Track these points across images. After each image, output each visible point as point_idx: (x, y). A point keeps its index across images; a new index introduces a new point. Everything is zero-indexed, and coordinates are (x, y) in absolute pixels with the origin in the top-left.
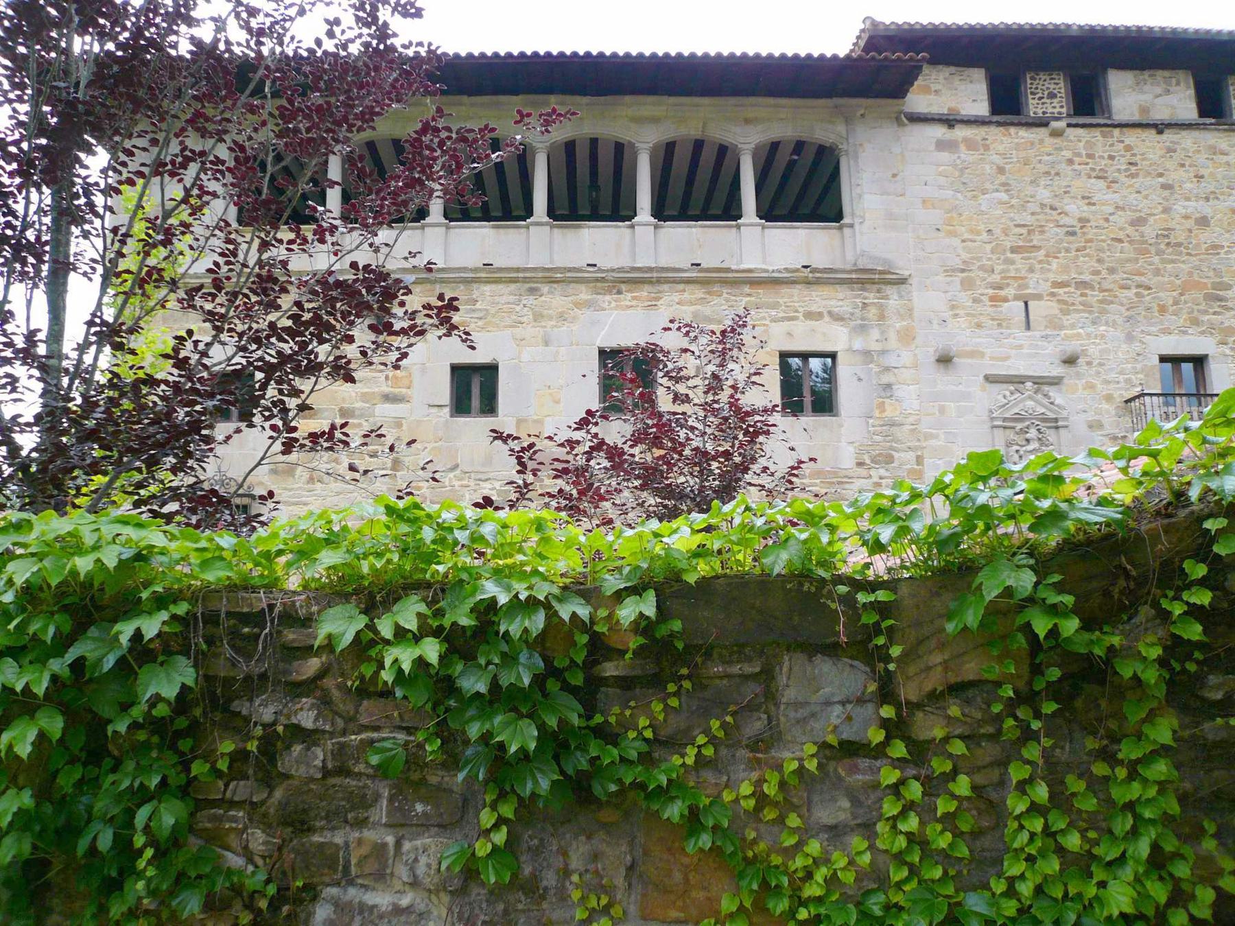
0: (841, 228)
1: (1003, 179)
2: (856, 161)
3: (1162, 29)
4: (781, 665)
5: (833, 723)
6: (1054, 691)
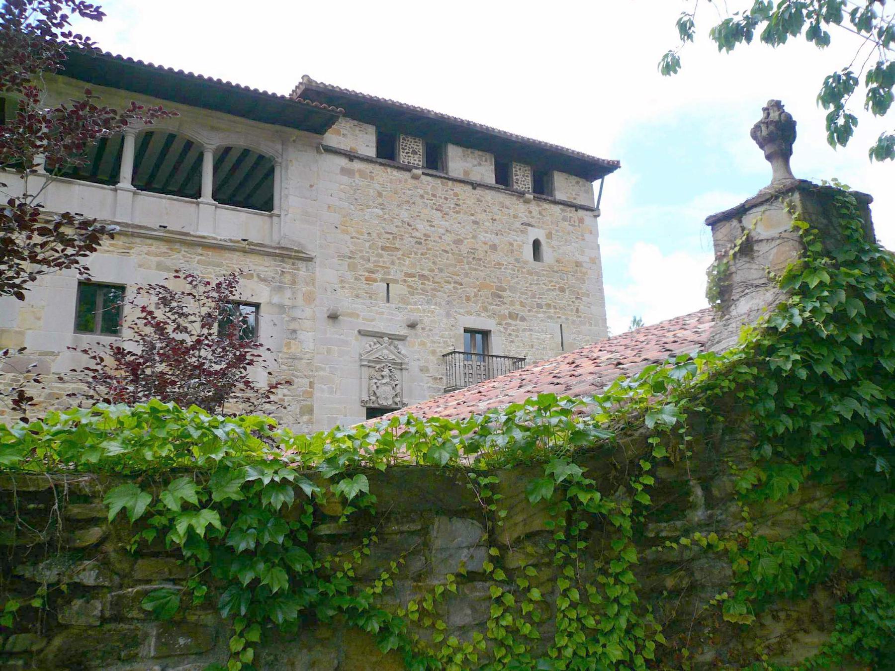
0: (271, 216)
1: (380, 200)
2: (286, 171)
3: (573, 151)
4: (433, 524)
5: (463, 561)
6: (584, 536)
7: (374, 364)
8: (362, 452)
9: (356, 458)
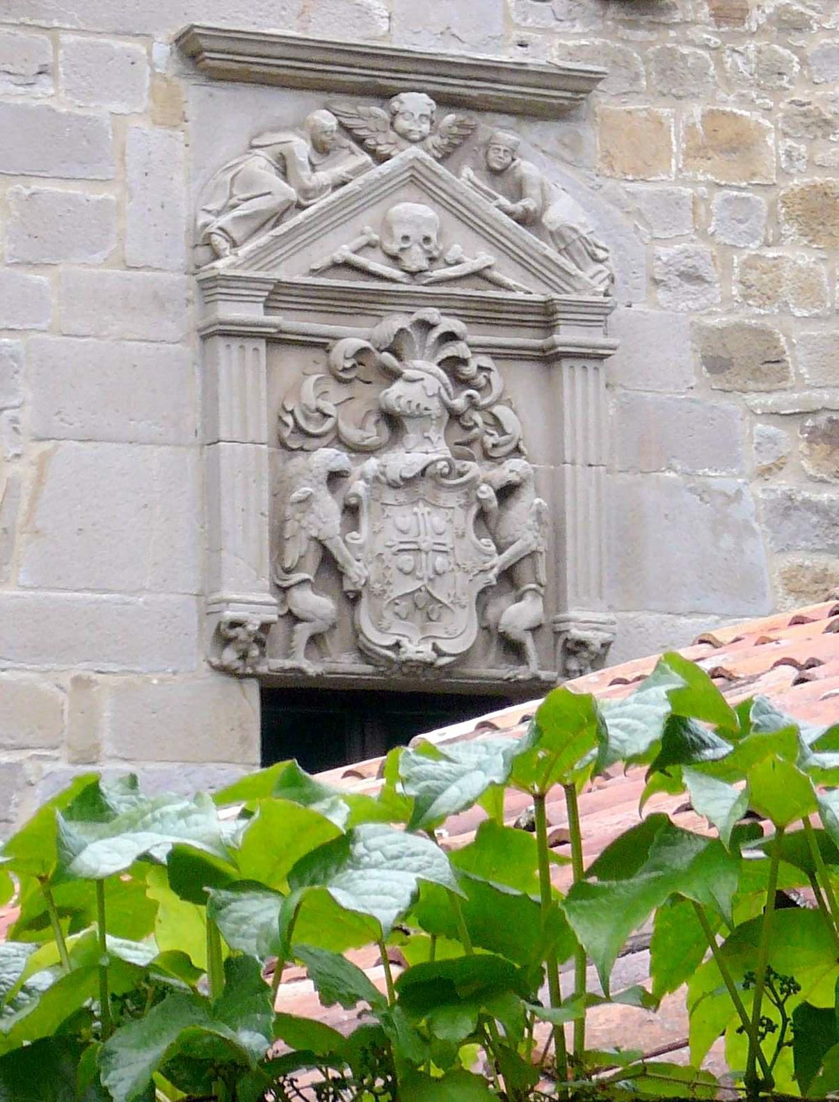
7: (311, 319)
8: (296, 994)
9: (250, 1039)
